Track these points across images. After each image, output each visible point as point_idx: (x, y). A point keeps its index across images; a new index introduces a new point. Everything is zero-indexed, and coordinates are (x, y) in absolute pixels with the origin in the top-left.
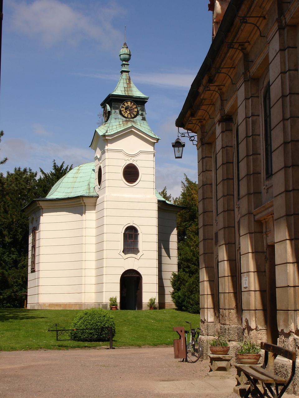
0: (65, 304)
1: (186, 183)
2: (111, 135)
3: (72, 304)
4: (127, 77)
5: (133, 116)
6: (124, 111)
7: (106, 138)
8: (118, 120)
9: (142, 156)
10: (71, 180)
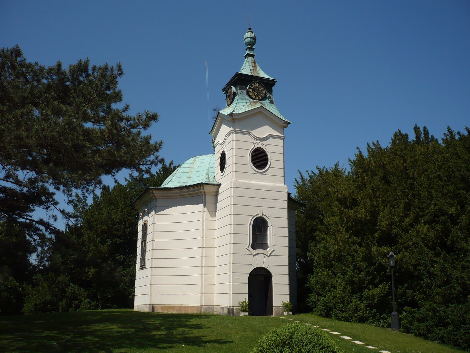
0: (179, 307)
1: (300, 181)
2: (239, 114)
3: (188, 307)
4: (252, 60)
5: (261, 98)
6: (252, 92)
9: (271, 141)
10: (187, 170)
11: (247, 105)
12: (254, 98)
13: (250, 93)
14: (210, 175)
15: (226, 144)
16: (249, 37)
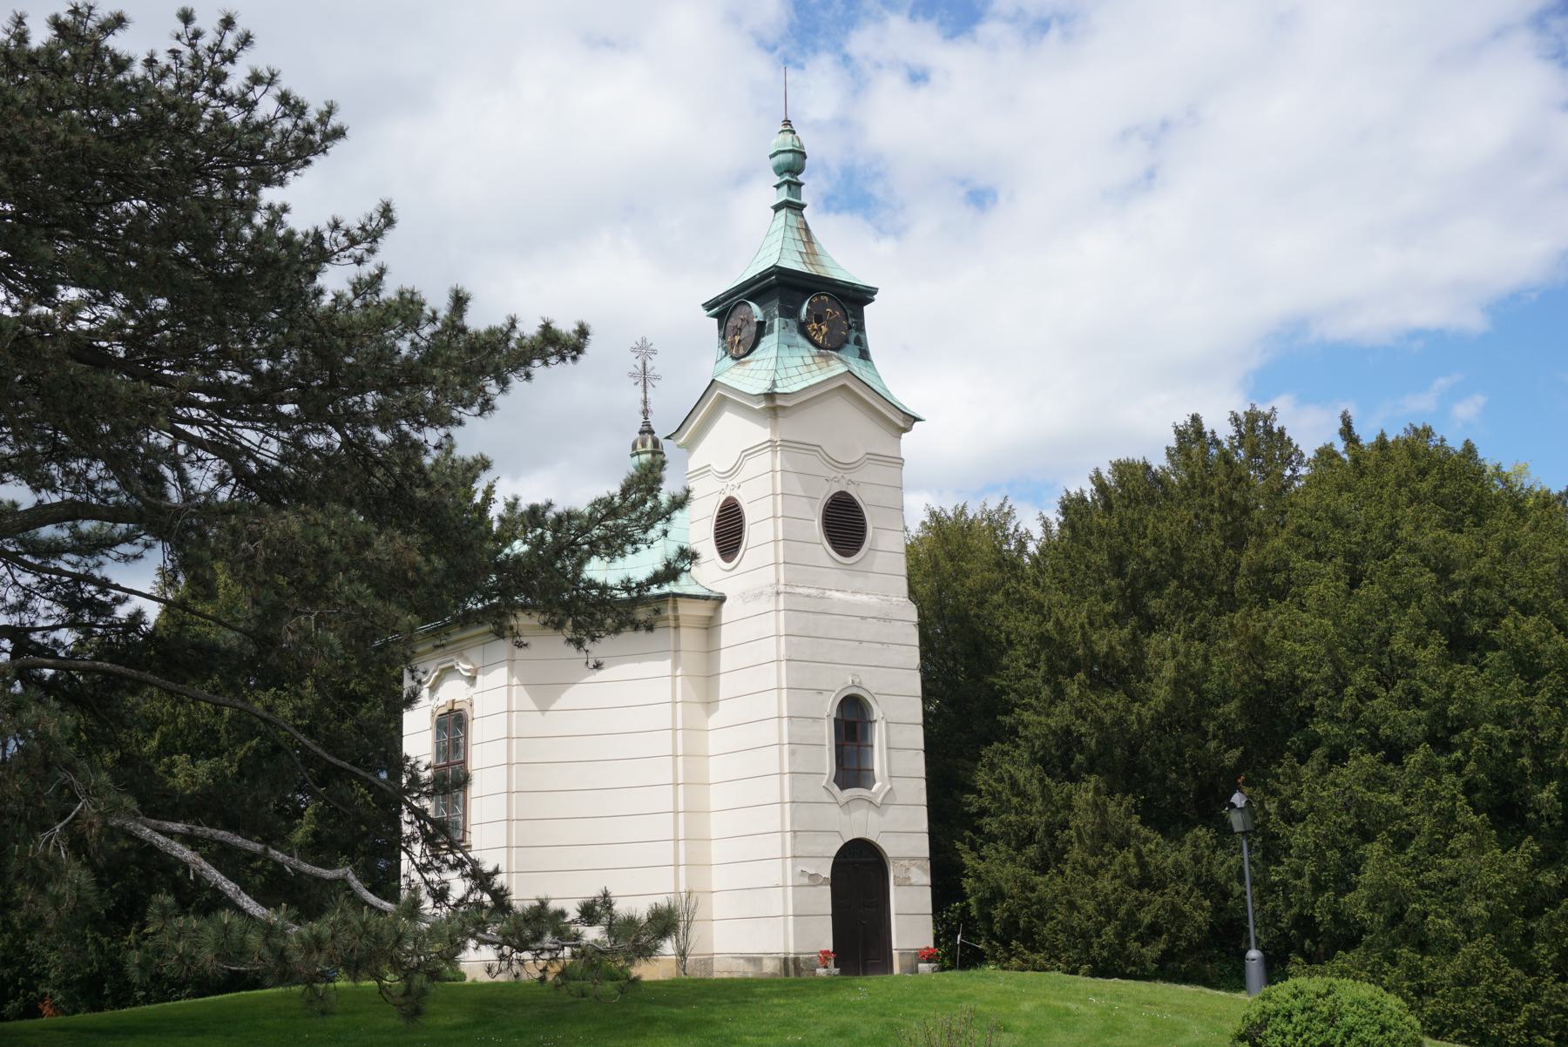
16: (790, 151)
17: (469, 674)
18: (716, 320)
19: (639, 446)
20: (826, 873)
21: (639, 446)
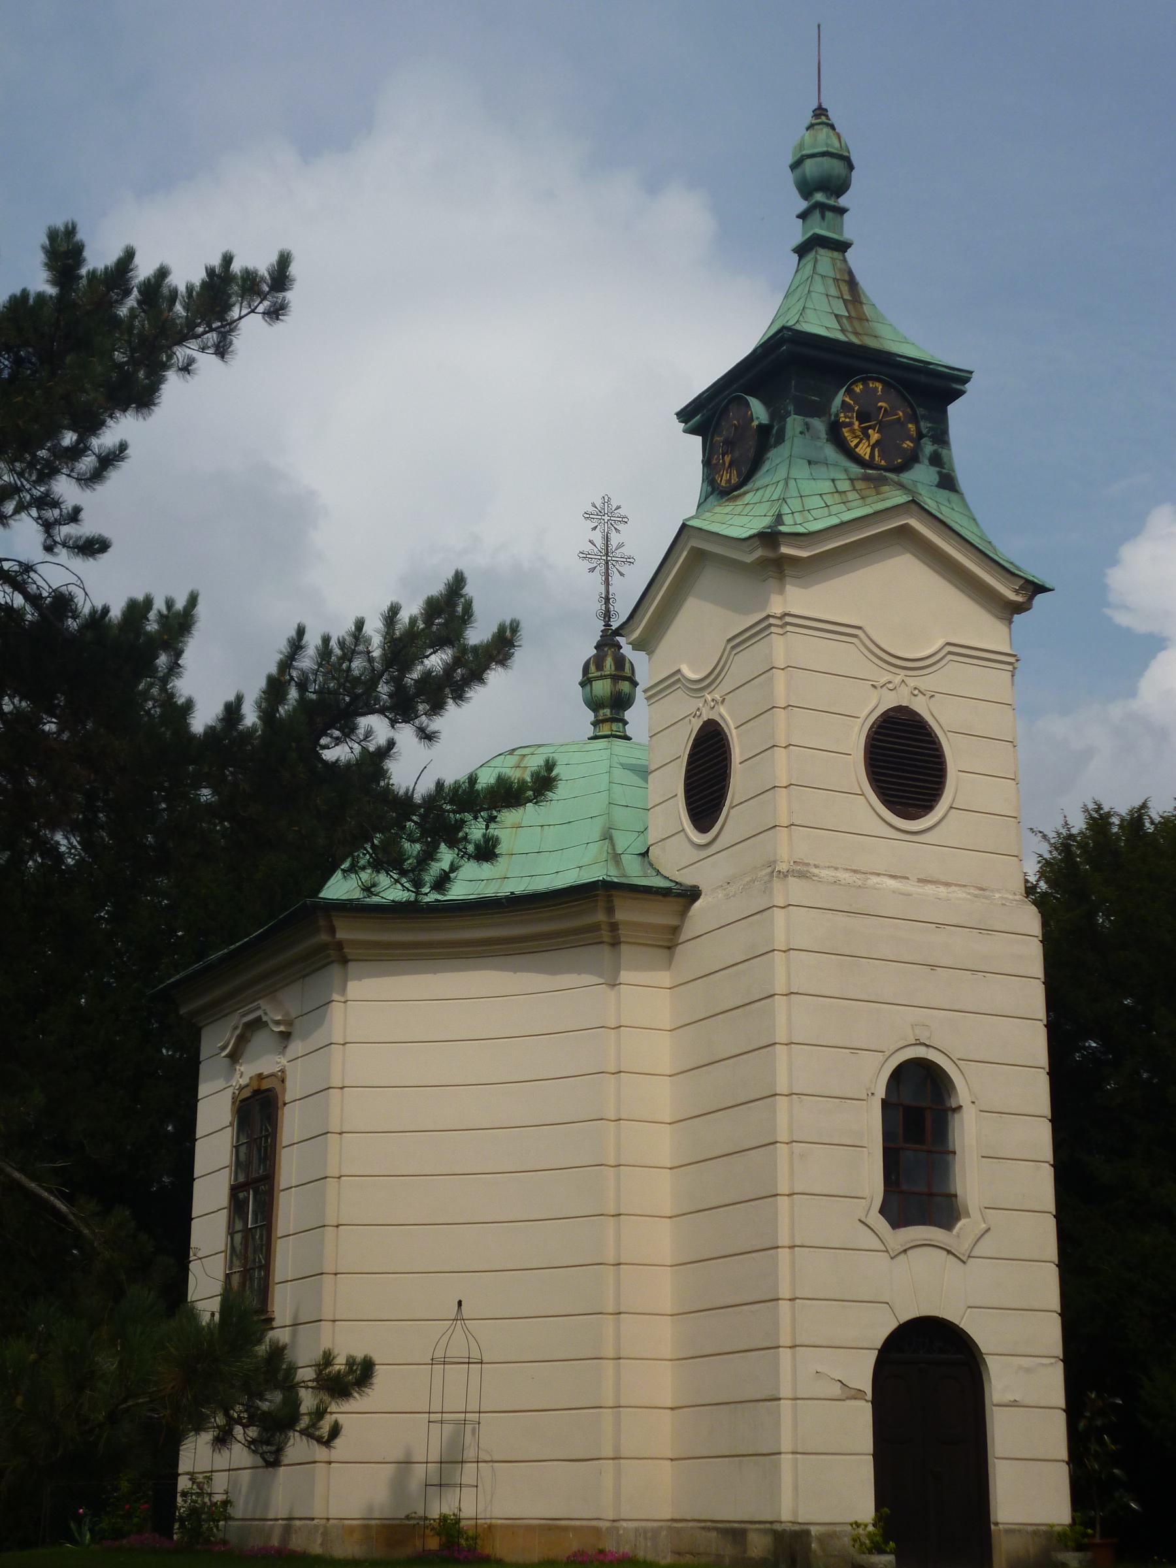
4: (840, 270)
7: (785, 550)
8: (823, 469)
11: (837, 492)
12: (867, 457)
13: (846, 432)
14: (623, 841)
15: (726, 685)
17: (282, 1028)
18: (698, 440)
19: (592, 668)
20: (865, 1382)
21: (592, 668)
